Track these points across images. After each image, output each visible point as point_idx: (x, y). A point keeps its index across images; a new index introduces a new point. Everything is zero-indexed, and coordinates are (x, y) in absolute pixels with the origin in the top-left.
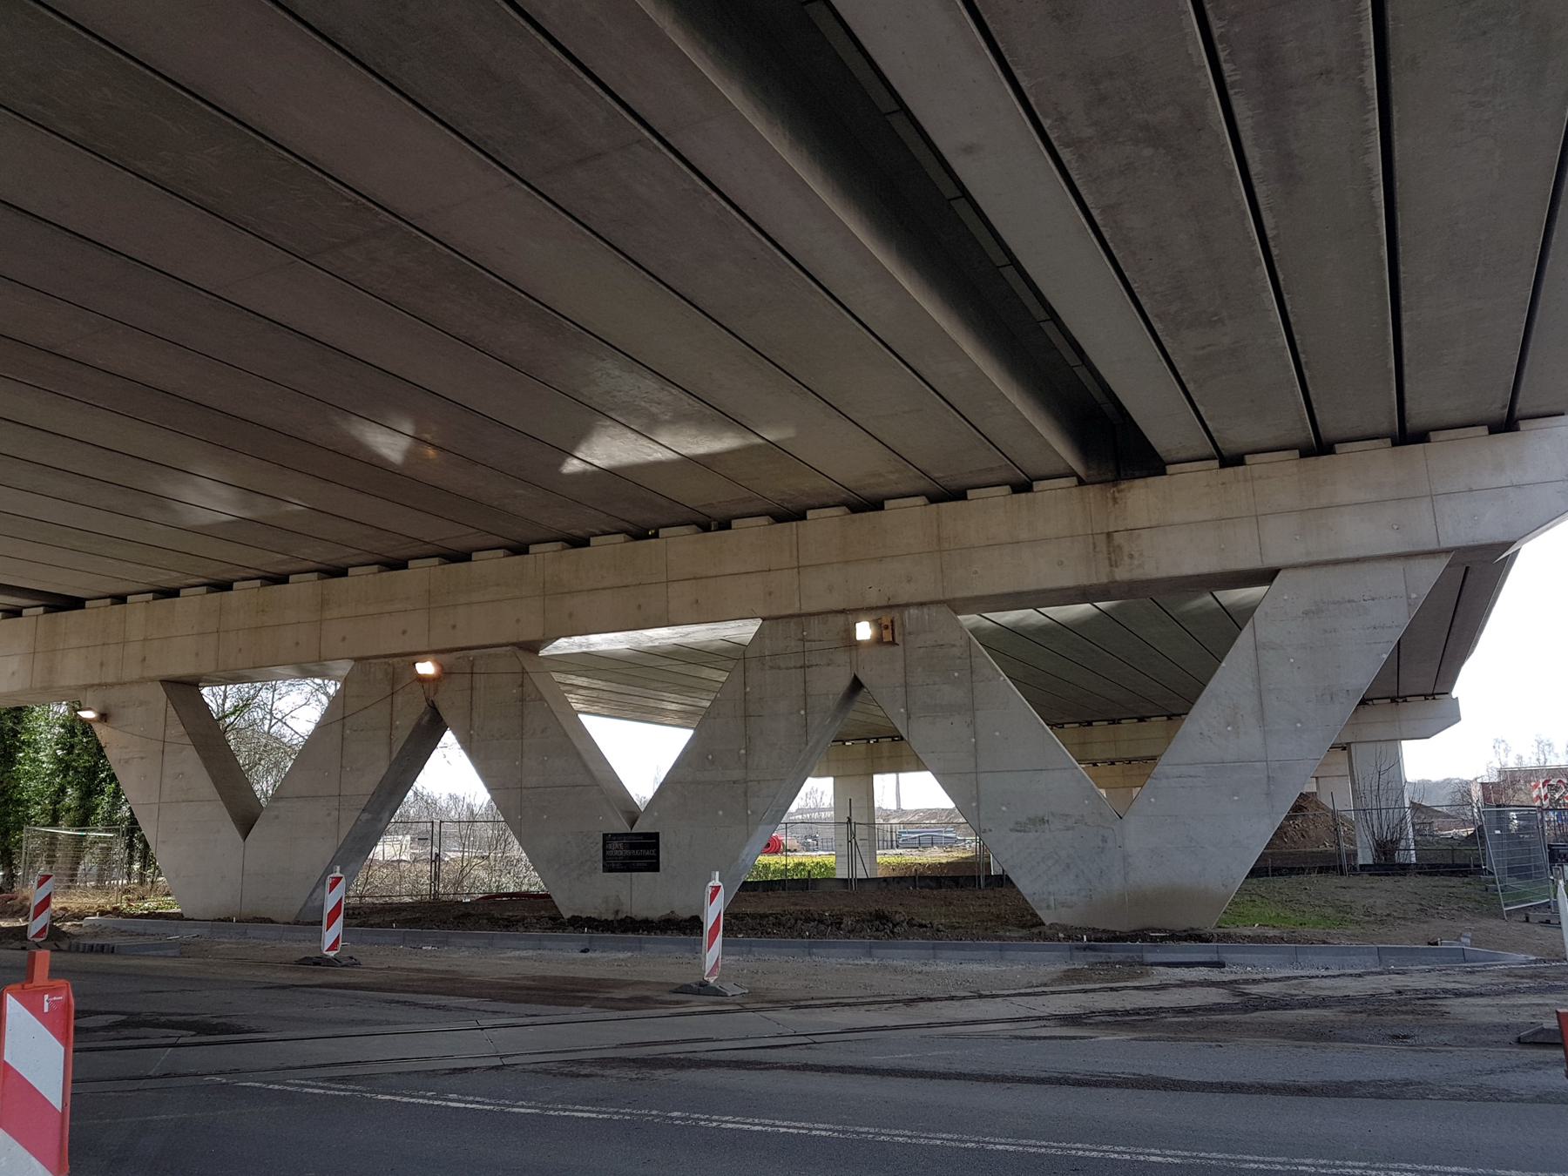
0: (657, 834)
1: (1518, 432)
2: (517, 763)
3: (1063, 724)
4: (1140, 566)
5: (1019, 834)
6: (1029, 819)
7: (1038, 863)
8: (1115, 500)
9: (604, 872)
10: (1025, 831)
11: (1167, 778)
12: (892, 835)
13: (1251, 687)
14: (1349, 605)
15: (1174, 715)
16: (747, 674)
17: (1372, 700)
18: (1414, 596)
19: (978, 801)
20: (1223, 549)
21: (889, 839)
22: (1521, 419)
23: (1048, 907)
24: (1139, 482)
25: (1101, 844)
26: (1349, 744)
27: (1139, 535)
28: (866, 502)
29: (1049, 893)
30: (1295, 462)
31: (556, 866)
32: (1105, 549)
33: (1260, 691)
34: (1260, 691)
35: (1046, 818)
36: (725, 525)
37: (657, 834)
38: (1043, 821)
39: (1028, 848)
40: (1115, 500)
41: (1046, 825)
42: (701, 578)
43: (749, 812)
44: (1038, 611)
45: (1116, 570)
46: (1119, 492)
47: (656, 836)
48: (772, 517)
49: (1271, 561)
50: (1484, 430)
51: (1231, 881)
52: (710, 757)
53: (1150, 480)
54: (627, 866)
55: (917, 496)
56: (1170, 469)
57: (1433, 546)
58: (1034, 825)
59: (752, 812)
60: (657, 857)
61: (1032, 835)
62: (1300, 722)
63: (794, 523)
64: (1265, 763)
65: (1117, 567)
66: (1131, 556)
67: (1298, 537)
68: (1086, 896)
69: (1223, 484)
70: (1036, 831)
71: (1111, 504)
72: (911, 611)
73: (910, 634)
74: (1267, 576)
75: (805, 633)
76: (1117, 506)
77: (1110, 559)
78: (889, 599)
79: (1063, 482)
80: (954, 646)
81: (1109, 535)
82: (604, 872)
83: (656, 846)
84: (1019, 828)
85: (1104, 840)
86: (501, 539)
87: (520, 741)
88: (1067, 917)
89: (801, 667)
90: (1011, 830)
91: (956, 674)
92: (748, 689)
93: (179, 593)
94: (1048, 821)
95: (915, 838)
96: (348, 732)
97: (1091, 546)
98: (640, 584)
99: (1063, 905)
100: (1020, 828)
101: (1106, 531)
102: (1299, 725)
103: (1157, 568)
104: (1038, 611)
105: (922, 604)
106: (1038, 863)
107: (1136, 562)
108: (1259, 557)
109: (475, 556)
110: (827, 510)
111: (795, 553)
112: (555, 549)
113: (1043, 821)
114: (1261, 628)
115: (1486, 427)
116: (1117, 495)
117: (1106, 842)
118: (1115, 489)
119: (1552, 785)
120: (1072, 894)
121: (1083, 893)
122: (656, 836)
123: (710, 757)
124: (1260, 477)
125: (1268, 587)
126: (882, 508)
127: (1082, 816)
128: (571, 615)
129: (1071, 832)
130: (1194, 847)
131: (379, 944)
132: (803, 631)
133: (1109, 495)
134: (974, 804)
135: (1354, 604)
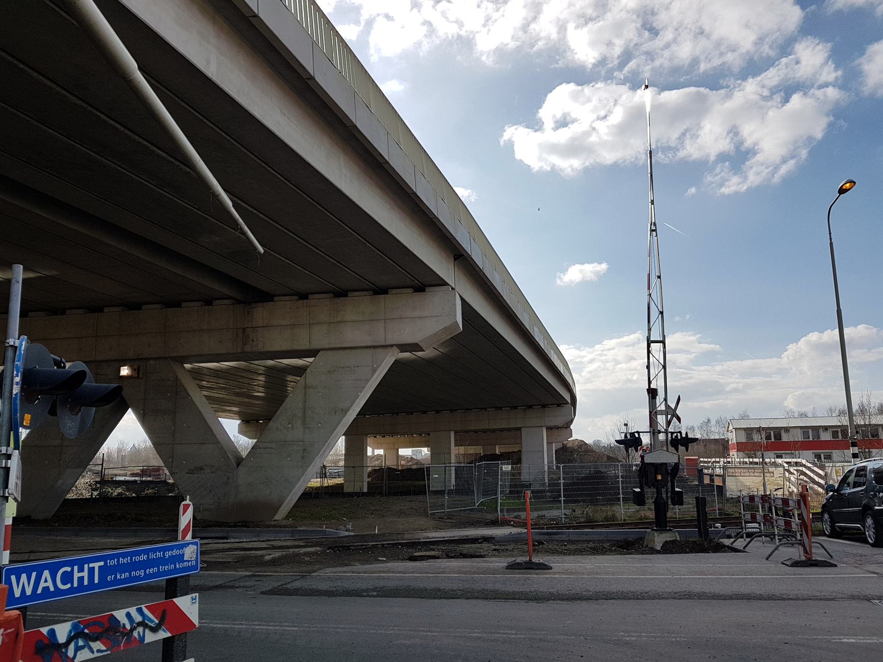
1: (424, 293)
3: (398, 413)
6: (195, 468)
7: (197, 489)
10: (193, 474)
13: (301, 406)
14: (347, 369)
15: (454, 410)
17: (548, 405)
18: (375, 366)
19: (173, 458)
26: (521, 428)
27: (258, 331)
28: (421, 285)
29: (201, 504)
32: (241, 336)
33: (305, 408)
34: (305, 408)
36: (63, 313)
38: (202, 469)
44: (413, 354)
45: (245, 346)
46: (250, 308)
48: (333, 294)
49: (315, 345)
53: (265, 304)
55: (409, 288)
56: (276, 298)
57: (383, 344)
61: (196, 476)
62: (321, 423)
63: (97, 314)
64: (303, 443)
65: (246, 345)
66: (253, 340)
67: (326, 336)
69: (297, 308)
70: (198, 474)
72: (151, 362)
73: (150, 373)
74: (313, 353)
75: (98, 371)
76: (249, 315)
77: (243, 341)
78: (138, 355)
79: (226, 302)
80: (169, 380)
81: (244, 329)
85: (228, 478)
86: (292, 291)
90: (187, 473)
91: (169, 394)
93: (103, 310)
95: (336, 472)
97: (235, 334)
100: (191, 472)
101: (243, 327)
102: (320, 425)
103: (264, 346)
104: (413, 354)
105: (156, 359)
107: (254, 343)
108: (308, 344)
109: (310, 296)
113: (202, 469)
114: (310, 378)
116: (250, 310)
118: (249, 307)
119: (644, 450)
120: (210, 505)
121: (216, 504)
123: (44, 433)
124: (313, 306)
125: (314, 358)
129: (213, 474)
130: (268, 482)
132: (98, 370)
134: (170, 460)
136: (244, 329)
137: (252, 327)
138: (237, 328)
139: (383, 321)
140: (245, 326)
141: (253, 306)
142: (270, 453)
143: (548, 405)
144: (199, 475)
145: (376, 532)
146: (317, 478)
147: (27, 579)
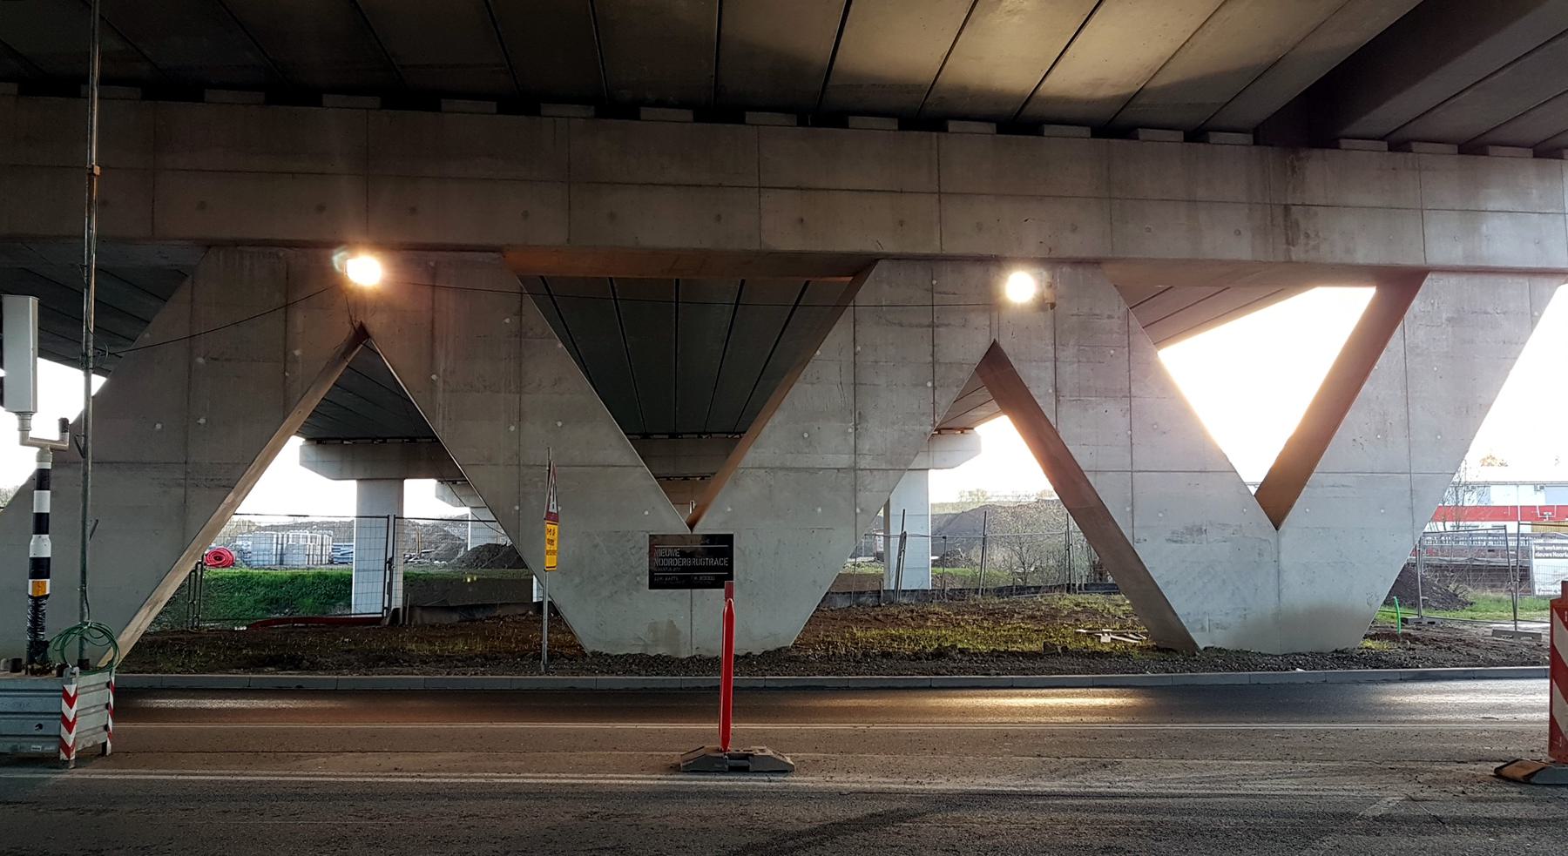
0: (731, 536)
2: (512, 428)
4: (1316, 248)
5: (1174, 545)
6: (1187, 529)
8: (1294, 171)
9: (650, 588)
10: (1181, 542)
11: (1322, 486)
12: (322, 550)
16: (857, 328)
17: (681, 434)
20: (1390, 240)
21: (319, 553)
22: (1491, 145)
23: (1203, 629)
24: (1317, 153)
25: (1257, 559)
27: (1316, 214)
30: (1179, 144)
31: (577, 580)
35: (1204, 528)
37: (731, 536)
38: (1200, 531)
39: (1183, 561)
40: (1294, 171)
41: (1204, 536)
42: (810, 189)
43: (858, 510)
47: (728, 539)
50: (1086, 131)
51: (1375, 599)
52: (806, 435)
54: (686, 580)
58: (1191, 534)
59: (862, 510)
60: (730, 568)
62: (1440, 435)
63: (935, 134)
64: (1409, 475)
65: (1293, 246)
66: (1307, 236)
68: (1240, 617)
71: (1289, 173)
82: (650, 588)
83: (728, 553)
84: (1175, 539)
87: (518, 395)
88: (1219, 639)
89: (929, 326)
90: (1167, 540)
92: (859, 348)
94: (1206, 530)
96: (201, 360)
98: (720, 185)
99: (1218, 626)
101: (1284, 203)
102: (1439, 437)
106: (1194, 579)
110: (1063, 127)
111: (936, 177)
112: (584, 115)
113: (1200, 531)
115: (896, 120)
116: (1296, 163)
117: (1263, 556)
122: (728, 539)
126: (1040, 133)
127: (1241, 526)
128: (202, 206)
131: (681, 689)
133: (1288, 162)
135: (1489, 316)
136: (1287, 208)
137: (1303, 205)
138: (760, 187)
139: (757, 189)
140: (1289, 202)
141: (1302, 155)
142: (1343, 497)
143: (681, 434)
144: (1194, 545)
145: (1548, 667)
146: (537, 597)
147: (1554, 720)
